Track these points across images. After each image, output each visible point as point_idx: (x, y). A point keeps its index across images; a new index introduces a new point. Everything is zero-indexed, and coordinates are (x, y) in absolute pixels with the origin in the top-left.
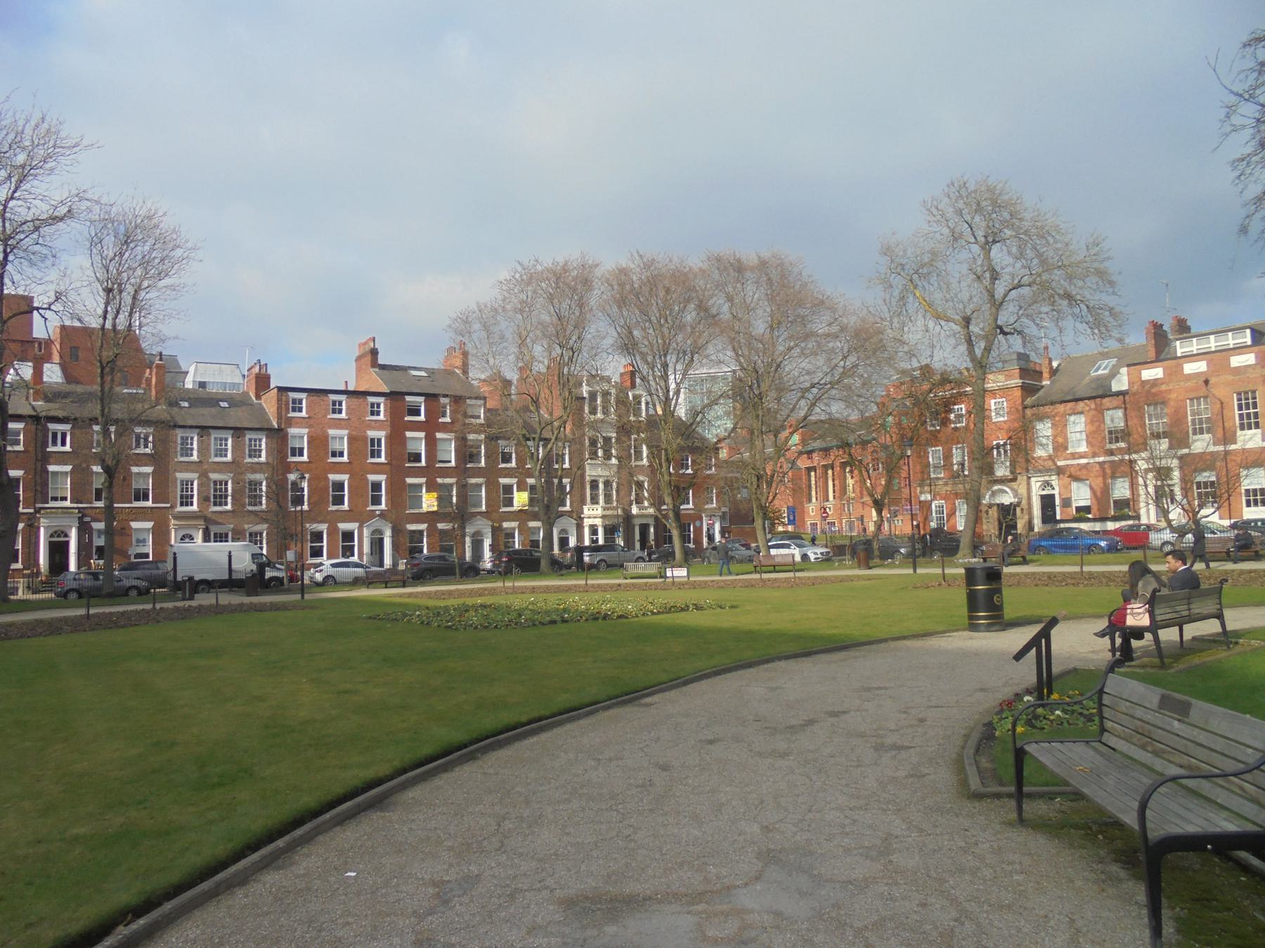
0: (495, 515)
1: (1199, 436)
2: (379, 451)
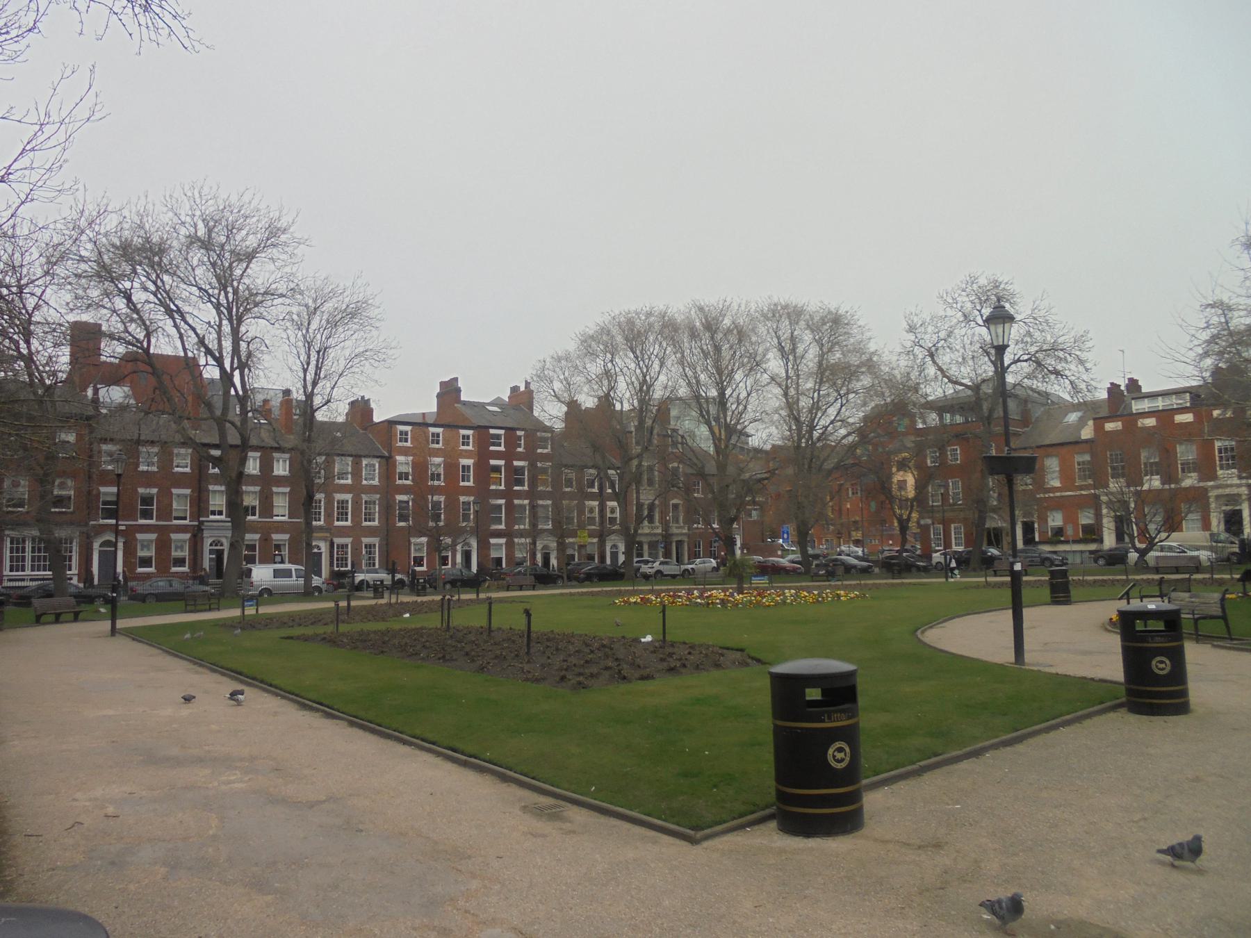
2: (469, 476)
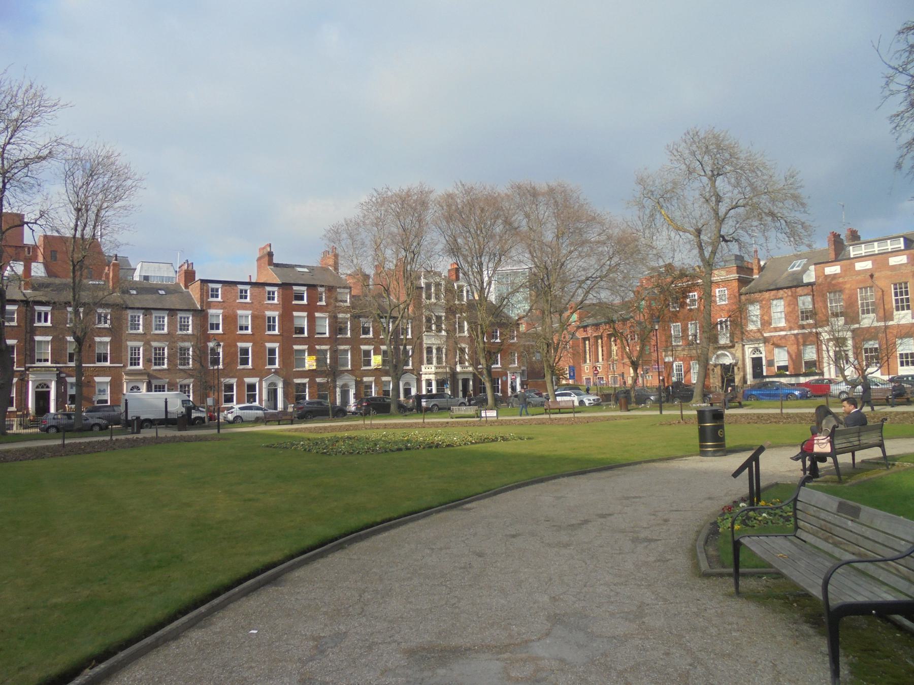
0: (357, 372)
1: (866, 315)
2: (274, 326)
